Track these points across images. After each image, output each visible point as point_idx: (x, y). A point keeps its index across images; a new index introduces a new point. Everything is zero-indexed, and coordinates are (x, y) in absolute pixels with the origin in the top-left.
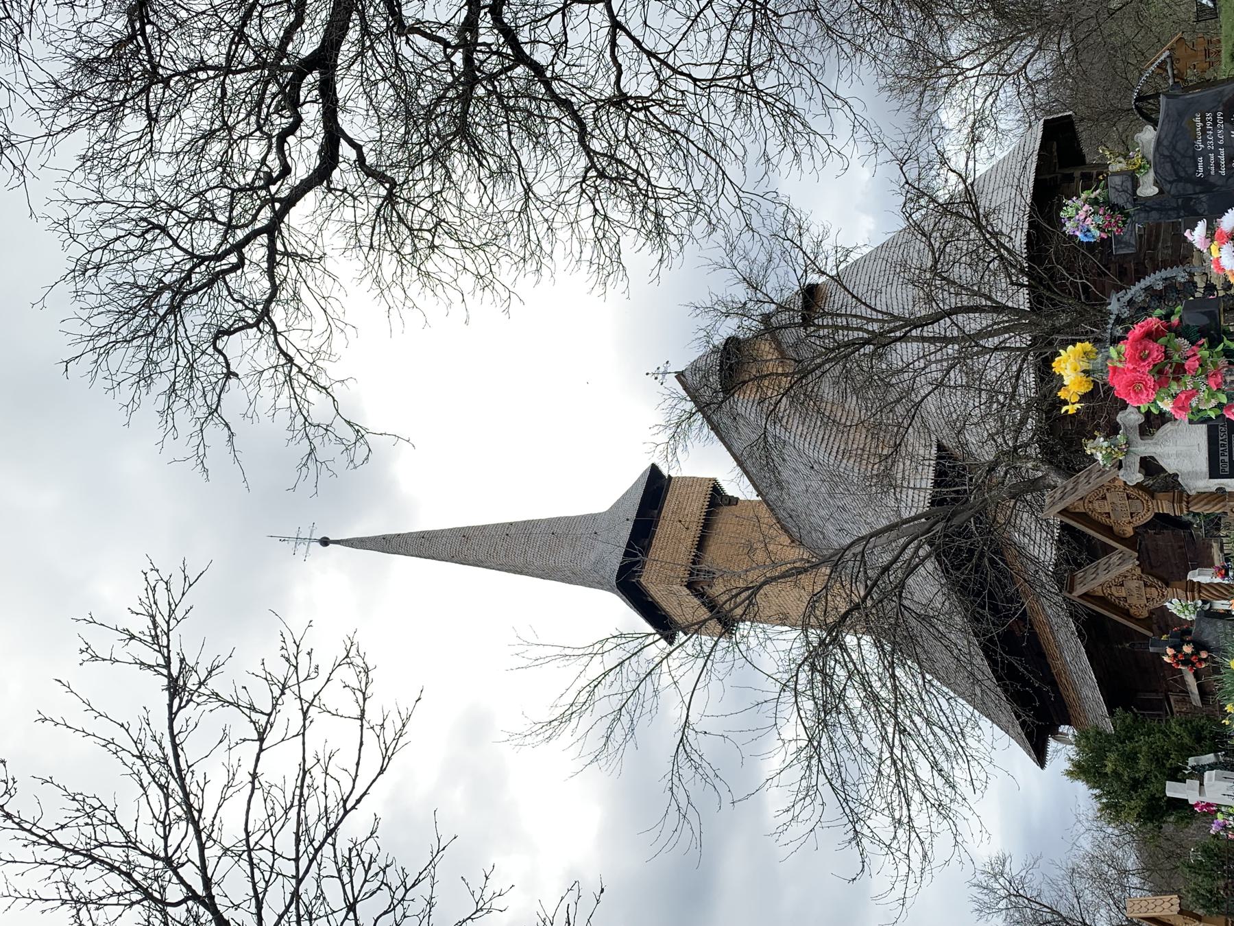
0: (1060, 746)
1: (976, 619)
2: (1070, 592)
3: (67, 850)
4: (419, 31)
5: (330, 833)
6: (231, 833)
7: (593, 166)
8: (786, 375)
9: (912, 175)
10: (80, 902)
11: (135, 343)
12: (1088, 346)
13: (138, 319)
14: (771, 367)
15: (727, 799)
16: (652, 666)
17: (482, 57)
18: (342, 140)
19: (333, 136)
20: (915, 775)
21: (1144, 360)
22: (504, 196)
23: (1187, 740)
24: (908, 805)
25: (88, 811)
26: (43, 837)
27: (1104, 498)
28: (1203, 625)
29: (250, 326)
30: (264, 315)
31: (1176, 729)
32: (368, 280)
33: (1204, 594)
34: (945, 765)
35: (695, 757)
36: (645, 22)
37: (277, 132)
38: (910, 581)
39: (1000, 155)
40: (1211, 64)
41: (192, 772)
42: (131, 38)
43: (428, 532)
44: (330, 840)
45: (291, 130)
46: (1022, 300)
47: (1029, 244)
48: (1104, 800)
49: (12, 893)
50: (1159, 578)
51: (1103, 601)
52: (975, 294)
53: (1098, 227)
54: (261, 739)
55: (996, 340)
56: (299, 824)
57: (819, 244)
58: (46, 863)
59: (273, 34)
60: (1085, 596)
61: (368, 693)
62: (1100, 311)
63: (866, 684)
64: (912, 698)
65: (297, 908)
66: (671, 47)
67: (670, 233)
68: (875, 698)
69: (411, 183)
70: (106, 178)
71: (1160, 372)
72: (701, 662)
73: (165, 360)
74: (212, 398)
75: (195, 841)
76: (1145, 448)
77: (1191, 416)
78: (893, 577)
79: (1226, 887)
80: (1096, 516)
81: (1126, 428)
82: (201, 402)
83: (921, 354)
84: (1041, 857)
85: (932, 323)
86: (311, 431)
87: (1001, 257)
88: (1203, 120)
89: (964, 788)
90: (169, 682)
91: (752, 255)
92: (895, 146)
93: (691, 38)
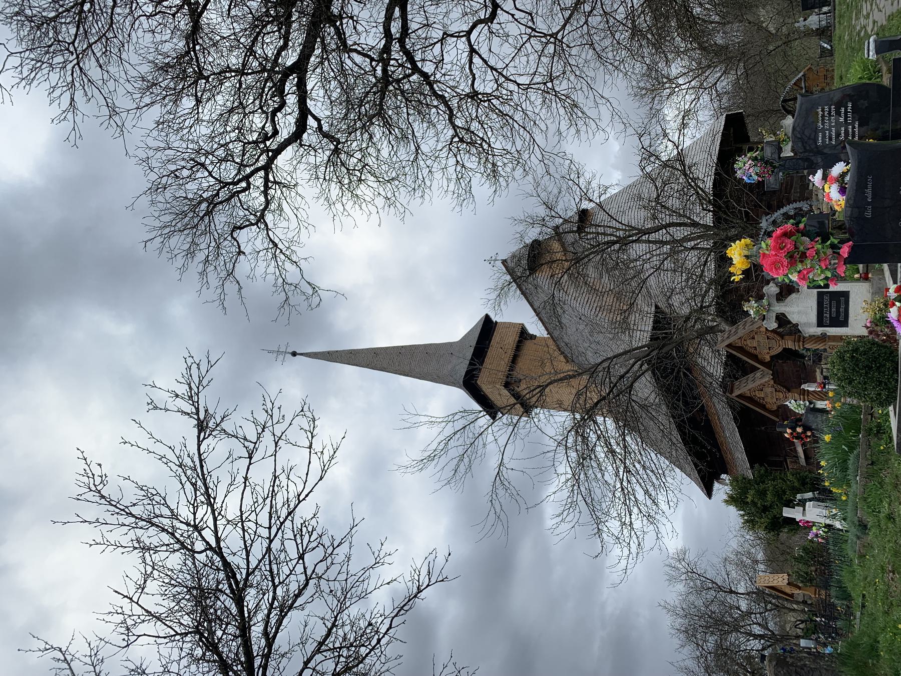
0: (721, 486)
1: (672, 407)
2: (731, 393)
3: (137, 518)
4: (356, 51)
5: (289, 514)
6: (232, 512)
7: (457, 135)
8: (566, 260)
9: (646, 143)
10: (145, 549)
11: (186, 232)
12: (748, 241)
13: (187, 219)
14: (559, 256)
15: (523, 506)
16: (482, 430)
17: (392, 69)
18: (309, 117)
19: (304, 112)
20: (635, 498)
21: (782, 249)
22: (404, 152)
23: (796, 484)
24: (630, 515)
25: (150, 495)
26: (123, 510)
27: (753, 338)
28: (809, 415)
29: (253, 224)
30: (261, 218)
31: (790, 477)
32: (322, 200)
33: (811, 397)
34: (653, 493)
35: (506, 483)
36: (490, 49)
37: (271, 109)
38: (636, 385)
39: (698, 136)
40: (828, 84)
41: (211, 476)
42: (187, 53)
43: (354, 350)
44: (290, 518)
45: (279, 109)
46: (709, 219)
47: (714, 184)
48: (746, 518)
49: (106, 543)
50: (785, 387)
51: (750, 399)
52: (680, 215)
53: (757, 174)
54: (250, 458)
55: (693, 243)
56: (271, 507)
57: (589, 183)
58: (125, 525)
59: (270, 52)
60: (740, 396)
61: (315, 433)
62: (756, 227)
63: (608, 444)
64: (635, 453)
65: (269, 556)
66: (505, 65)
67: (501, 176)
68: (613, 452)
69: (349, 143)
70: (171, 134)
71: (792, 257)
72: (511, 428)
73: (203, 242)
74: (230, 266)
75: (211, 516)
76: (779, 308)
77: (809, 284)
78: (626, 382)
79: (816, 570)
80: (748, 349)
81: (768, 296)
82: (223, 268)
83: (648, 251)
84: (707, 550)
85: (655, 232)
86: (287, 287)
87: (698, 193)
88: (823, 110)
89: (663, 506)
90: (198, 423)
91: (549, 189)
92: (636, 125)
93: (517, 61)
